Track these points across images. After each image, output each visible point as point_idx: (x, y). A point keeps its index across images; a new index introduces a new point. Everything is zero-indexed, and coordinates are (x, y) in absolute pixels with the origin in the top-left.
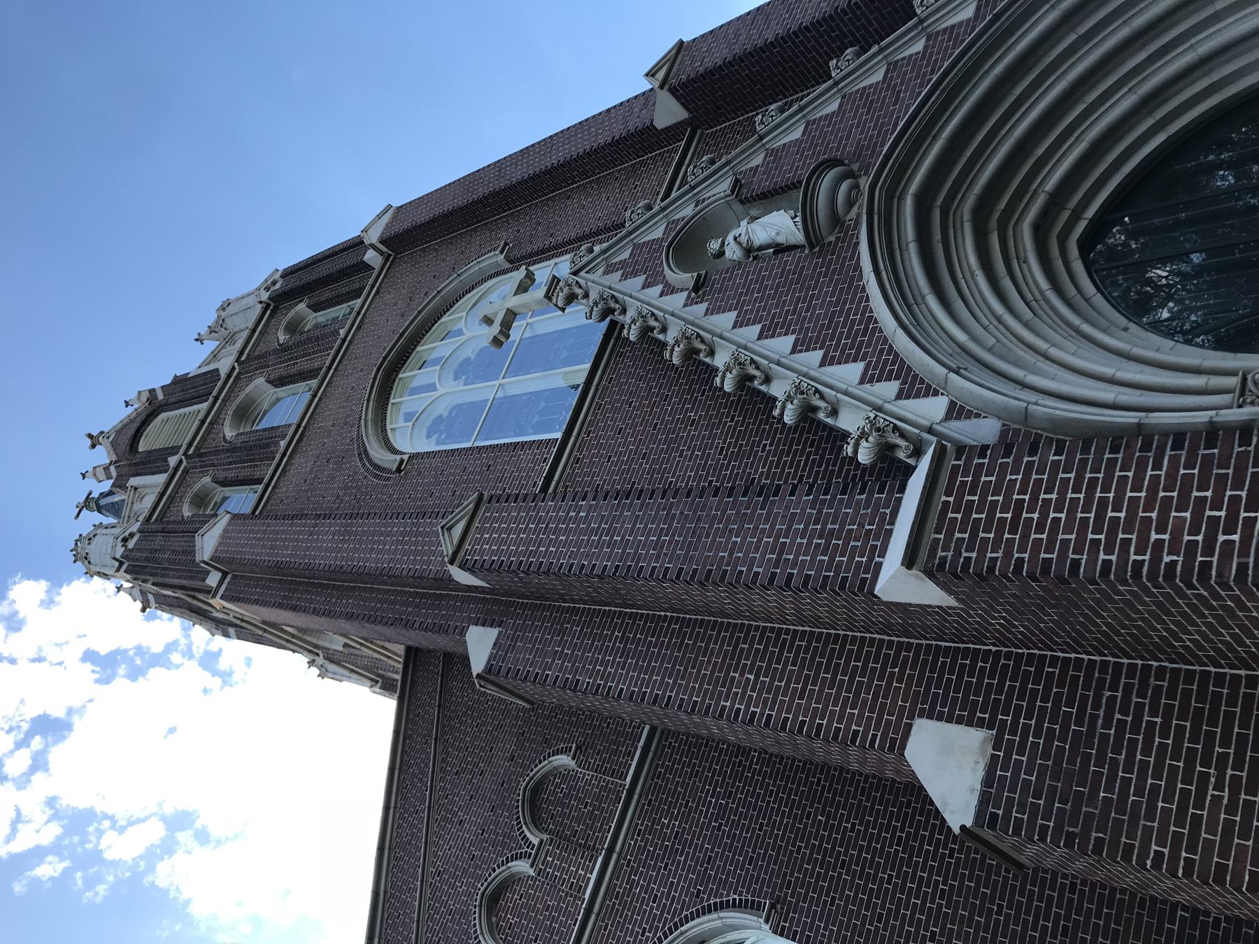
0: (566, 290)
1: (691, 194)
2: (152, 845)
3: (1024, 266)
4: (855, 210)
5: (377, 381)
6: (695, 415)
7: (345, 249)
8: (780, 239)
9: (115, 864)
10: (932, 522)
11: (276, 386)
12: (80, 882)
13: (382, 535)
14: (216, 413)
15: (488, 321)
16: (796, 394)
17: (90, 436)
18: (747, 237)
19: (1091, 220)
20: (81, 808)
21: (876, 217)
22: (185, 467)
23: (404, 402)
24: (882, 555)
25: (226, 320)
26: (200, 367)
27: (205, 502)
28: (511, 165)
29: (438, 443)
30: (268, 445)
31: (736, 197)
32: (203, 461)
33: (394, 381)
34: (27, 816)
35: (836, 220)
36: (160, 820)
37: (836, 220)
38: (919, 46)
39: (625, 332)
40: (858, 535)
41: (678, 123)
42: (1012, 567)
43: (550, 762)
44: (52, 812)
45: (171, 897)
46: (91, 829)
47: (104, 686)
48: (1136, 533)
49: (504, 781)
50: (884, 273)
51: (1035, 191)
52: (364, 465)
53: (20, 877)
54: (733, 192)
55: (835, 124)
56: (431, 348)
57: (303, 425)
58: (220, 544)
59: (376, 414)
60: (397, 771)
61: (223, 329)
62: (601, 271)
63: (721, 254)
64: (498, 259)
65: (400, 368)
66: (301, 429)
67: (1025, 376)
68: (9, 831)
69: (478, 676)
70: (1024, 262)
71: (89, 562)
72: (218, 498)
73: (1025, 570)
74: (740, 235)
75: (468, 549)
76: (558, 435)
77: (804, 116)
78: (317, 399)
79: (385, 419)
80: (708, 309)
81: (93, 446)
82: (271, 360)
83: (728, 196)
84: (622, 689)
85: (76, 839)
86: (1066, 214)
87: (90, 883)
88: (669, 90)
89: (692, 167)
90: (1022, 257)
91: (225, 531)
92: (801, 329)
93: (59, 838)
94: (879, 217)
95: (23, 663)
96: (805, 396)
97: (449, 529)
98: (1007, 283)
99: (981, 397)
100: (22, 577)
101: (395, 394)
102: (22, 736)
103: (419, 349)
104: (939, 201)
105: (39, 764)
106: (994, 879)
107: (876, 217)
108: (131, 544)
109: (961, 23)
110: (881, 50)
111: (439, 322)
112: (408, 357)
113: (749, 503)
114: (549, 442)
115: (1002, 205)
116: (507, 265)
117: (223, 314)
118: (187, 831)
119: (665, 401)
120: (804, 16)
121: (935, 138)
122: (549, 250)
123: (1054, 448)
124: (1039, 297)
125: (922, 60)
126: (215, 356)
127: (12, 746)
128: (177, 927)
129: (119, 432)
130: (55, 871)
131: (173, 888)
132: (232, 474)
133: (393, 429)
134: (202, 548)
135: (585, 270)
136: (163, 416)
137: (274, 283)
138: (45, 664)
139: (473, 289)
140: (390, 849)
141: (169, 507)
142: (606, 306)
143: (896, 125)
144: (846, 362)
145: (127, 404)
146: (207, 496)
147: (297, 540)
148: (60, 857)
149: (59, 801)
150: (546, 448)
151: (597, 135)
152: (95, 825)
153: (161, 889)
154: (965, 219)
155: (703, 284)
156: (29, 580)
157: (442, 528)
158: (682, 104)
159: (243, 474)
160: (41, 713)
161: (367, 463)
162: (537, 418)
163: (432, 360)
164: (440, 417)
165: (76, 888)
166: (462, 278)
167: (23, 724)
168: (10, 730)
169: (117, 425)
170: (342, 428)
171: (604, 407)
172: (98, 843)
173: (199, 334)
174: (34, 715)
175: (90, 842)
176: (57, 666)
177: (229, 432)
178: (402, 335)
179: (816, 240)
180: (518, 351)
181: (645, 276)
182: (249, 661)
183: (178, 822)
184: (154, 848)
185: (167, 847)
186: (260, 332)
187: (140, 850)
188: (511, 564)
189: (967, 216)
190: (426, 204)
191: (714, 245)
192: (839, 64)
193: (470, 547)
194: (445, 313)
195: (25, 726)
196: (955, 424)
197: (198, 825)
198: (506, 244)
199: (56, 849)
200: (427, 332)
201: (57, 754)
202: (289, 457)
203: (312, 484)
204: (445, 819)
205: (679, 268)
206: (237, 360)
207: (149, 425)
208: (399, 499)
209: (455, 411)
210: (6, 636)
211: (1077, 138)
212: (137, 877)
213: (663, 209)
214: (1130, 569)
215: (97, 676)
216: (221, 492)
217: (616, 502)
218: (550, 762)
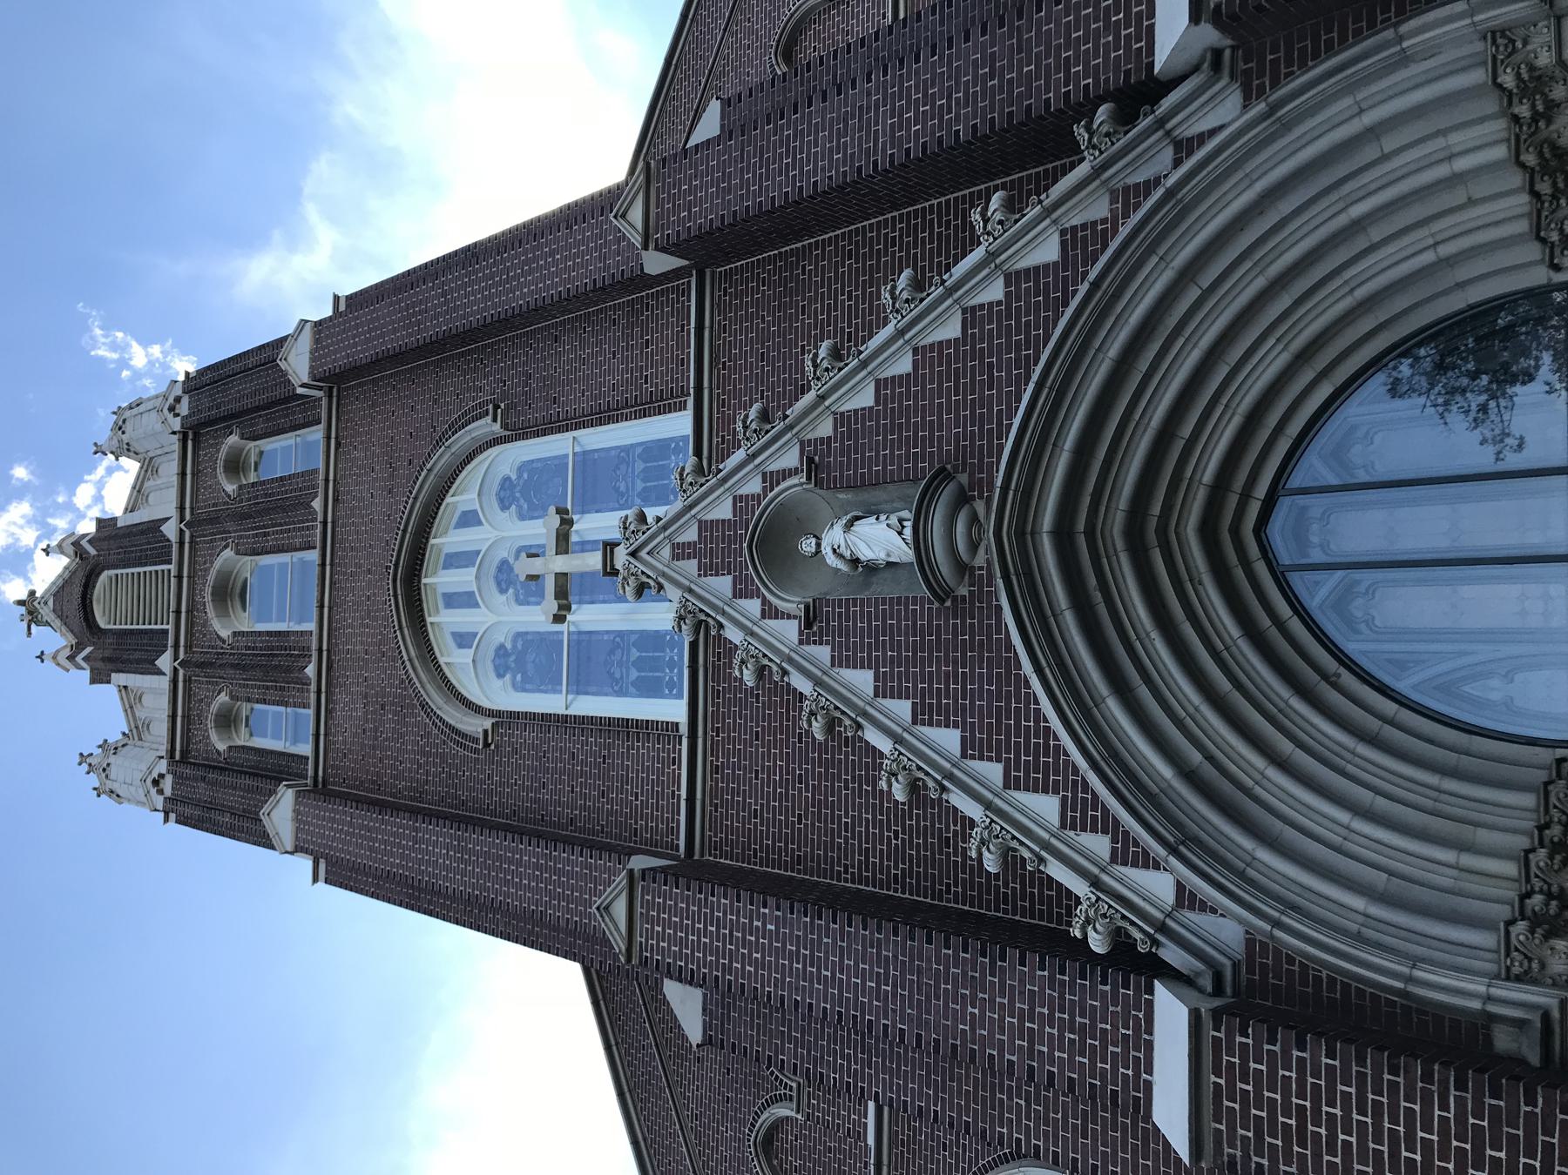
3: (1200, 588)
4: (981, 551)
5: (400, 597)
17: (81, 754)
22: (185, 675)
27: (232, 718)
33: (419, 589)
35: (962, 568)
37: (962, 568)
50: (1047, 671)
57: (325, 647)
59: (418, 646)
65: (420, 570)
66: (325, 653)
71: (107, 776)
74: (839, 547)
88: (657, 249)
94: (1017, 575)
104: (1081, 526)
112: (424, 555)
123: (1324, 1047)
133: (431, 623)
140: (630, 1091)
155: (815, 618)
157: (598, 908)
158: (678, 256)
162: (634, 674)
166: (453, 450)
178: (405, 531)
179: (945, 594)
186: (193, 474)
189: (1120, 544)
194: (447, 492)
200: (434, 518)
202: (326, 692)
204: (679, 1056)
207: (94, 587)
216: (245, 708)
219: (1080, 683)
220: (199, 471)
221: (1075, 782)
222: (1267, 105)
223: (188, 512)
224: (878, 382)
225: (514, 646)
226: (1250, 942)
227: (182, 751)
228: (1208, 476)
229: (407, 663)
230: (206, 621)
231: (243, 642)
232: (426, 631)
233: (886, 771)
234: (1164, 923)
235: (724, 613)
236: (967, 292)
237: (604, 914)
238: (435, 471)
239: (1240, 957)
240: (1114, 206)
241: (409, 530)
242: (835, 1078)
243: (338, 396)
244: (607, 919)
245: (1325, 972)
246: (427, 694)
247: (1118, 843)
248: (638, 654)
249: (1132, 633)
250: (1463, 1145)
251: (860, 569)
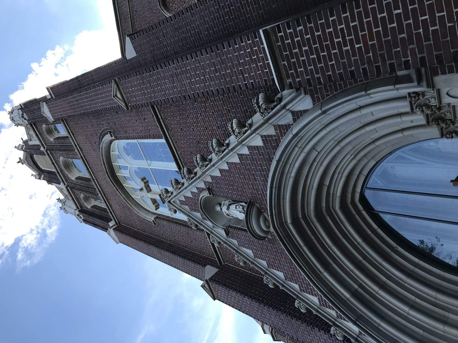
7: (103, 228)
37: (267, 233)
48: (339, 29)
59: (124, 194)
67: (379, 290)
71: (64, 205)
78: (95, 180)
104: (300, 216)
112: (113, 167)
141: (79, 201)
146: (66, 161)
155: (229, 232)
180: (144, 153)
182: (56, 75)
186: (40, 134)
189: (315, 220)
200: (110, 158)
202: (107, 201)
227: (80, 206)
228: (339, 193)
238: (103, 148)
241: (105, 163)
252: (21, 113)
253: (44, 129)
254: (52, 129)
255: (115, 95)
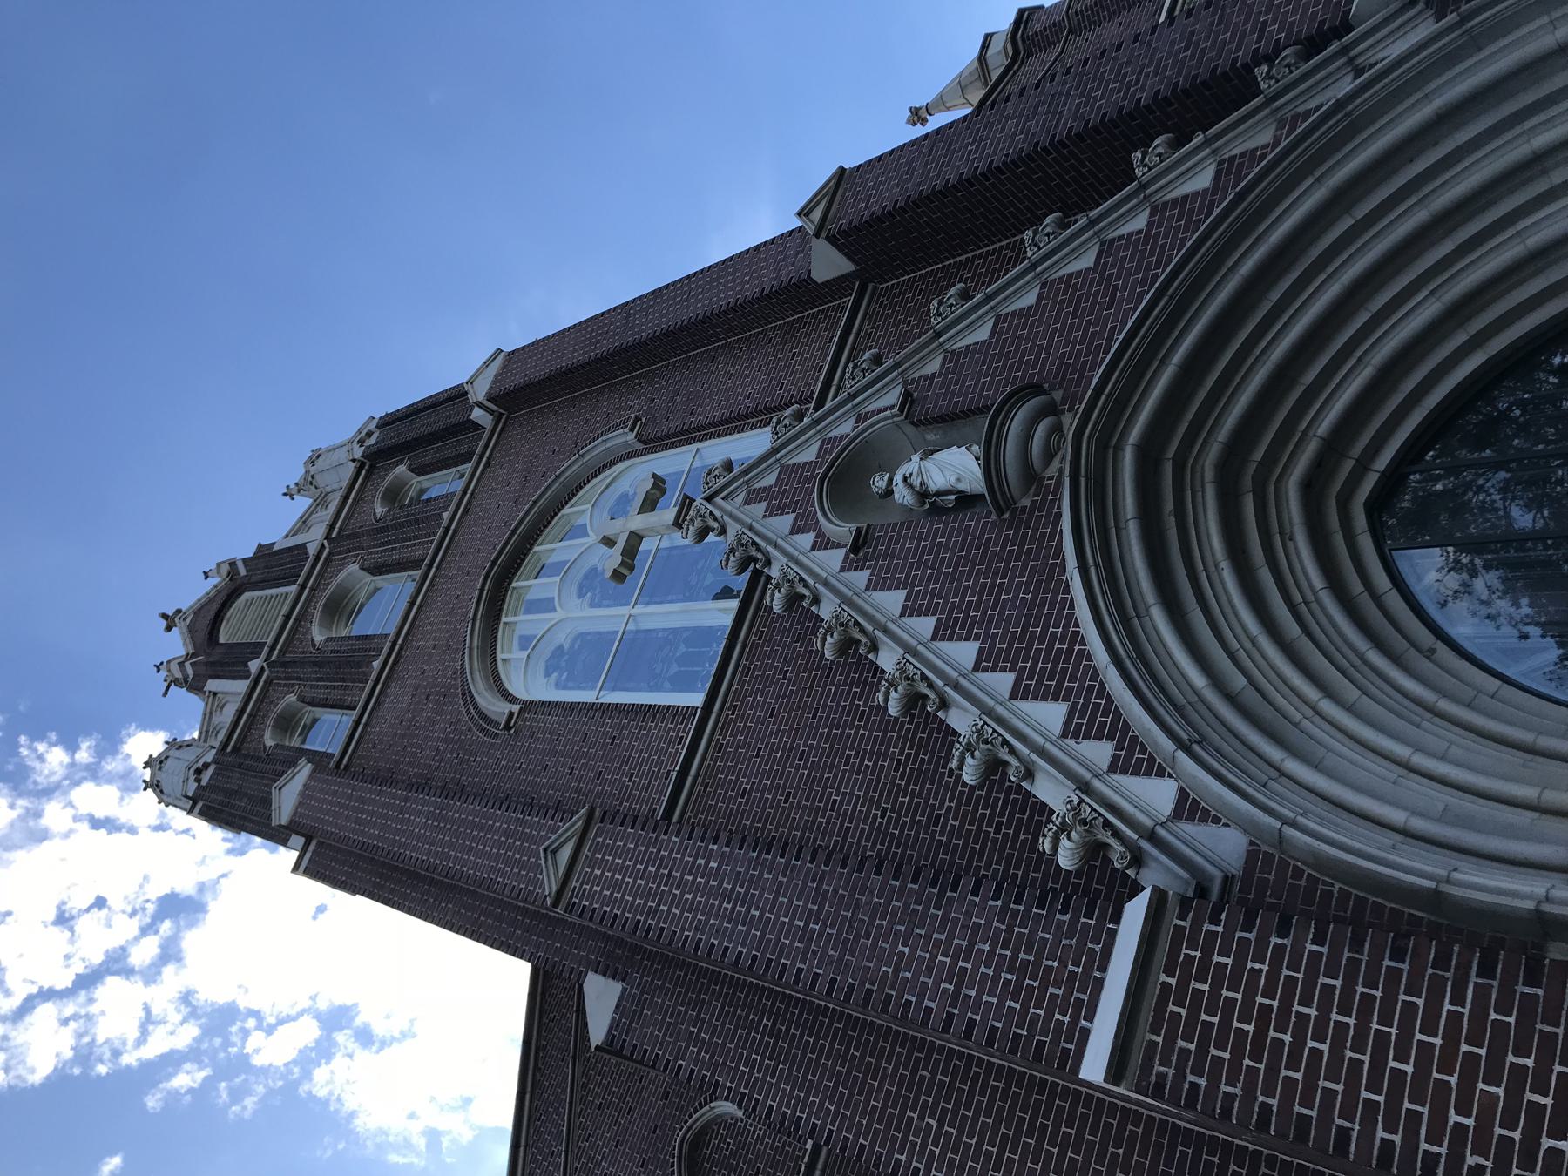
0: (698, 522)
1: (849, 406)
2: (306, 1047)
3: (1290, 544)
4: (1056, 463)
6: (865, 706)
7: (450, 399)
8: (962, 487)
9: (265, 1071)
10: (1147, 1014)
11: (372, 574)
12: (224, 1095)
13: (481, 830)
14: (302, 608)
15: (609, 542)
16: (978, 742)
17: (165, 616)
18: (920, 479)
19: (1383, 474)
20: (221, 1003)
21: (1083, 481)
22: (268, 677)
23: (518, 622)
24: (1090, 1017)
25: (316, 477)
26: (287, 536)
28: (641, 311)
29: (558, 686)
30: (358, 665)
31: (906, 418)
32: (288, 672)
33: (507, 591)
34: (158, 1015)
35: (1031, 477)
36: (314, 1018)
37: (1031, 477)
38: (1140, 222)
39: (768, 599)
40: (1059, 979)
41: (843, 276)
42: (1255, 1116)
43: (712, 1108)
44: (188, 1010)
45: (332, 1109)
46: (234, 1029)
47: (239, 858)
49: (656, 1126)
50: (1093, 570)
51: (1305, 433)
52: (468, 711)
53: (153, 1091)
54: (901, 410)
55: (1032, 326)
56: (549, 549)
57: (400, 642)
58: (300, 804)
59: (483, 638)
60: (528, 1096)
61: (313, 488)
62: (740, 499)
63: (889, 492)
64: (628, 438)
65: (514, 574)
66: (397, 647)
67: (1282, 760)
68: (138, 1034)
69: (597, 1048)
70: (1291, 540)
72: (306, 720)
73: (1273, 1127)
74: (911, 475)
75: (575, 887)
76: (696, 699)
77: (992, 308)
78: (415, 607)
79: (495, 645)
80: (870, 580)
81: (169, 628)
82: (366, 541)
83: (895, 415)
84: (771, 1107)
85: (217, 1041)
86: (1348, 465)
87: (237, 1095)
88: (827, 239)
89: (851, 365)
90: (1288, 531)
91: (306, 786)
92: (987, 634)
93: (197, 1040)
95: (144, 833)
96: (989, 746)
97: (554, 852)
98: (1265, 576)
99: (1220, 798)
100: (137, 728)
101: (507, 610)
102: (148, 920)
103: (536, 549)
104: (1171, 452)
105: (170, 954)
106: (1312, 1049)
107: (1083, 481)
108: (206, 777)
109: (1195, 194)
110: (1092, 223)
111: (560, 515)
112: (523, 560)
113: (920, 894)
114: (688, 711)
115: (1258, 455)
116: (640, 446)
117: (313, 470)
118: (346, 1031)
119: (828, 677)
120: (995, 152)
121: (1163, 362)
122: (689, 431)
123: (1312, 930)
124: (1310, 597)
125: (1146, 242)
126: (304, 522)
127: (136, 932)
128: (340, 1147)
129: (199, 611)
130: (194, 1082)
131: (333, 1098)
132: (321, 694)
133: (503, 660)
134: (279, 807)
135: (721, 496)
136: (247, 595)
137: (369, 434)
138: (170, 832)
139: (600, 473)
142: (746, 554)
143: (1110, 340)
144: (1044, 699)
145: (206, 575)
147: (386, 817)
148: (198, 1063)
149: (196, 996)
150: (682, 723)
151: (743, 283)
152: (239, 1023)
153: (320, 1099)
154: (1207, 480)
155: (865, 542)
156: (145, 730)
158: (845, 254)
159: (335, 695)
160: (169, 891)
161: (471, 708)
162: (674, 668)
163: (553, 564)
164: (561, 647)
165: (220, 1101)
167: (149, 906)
168: (133, 913)
169: (203, 597)
170: (444, 653)
171: (753, 674)
172: (243, 1047)
173: (288, 487)
174: (161, 893)
175: (234, 1045)
176: (184, 835)
177: (318, 635)
179: (1005, 502)
181: (794, 515)
183: (336, 1019)
184: (308, 1052)
185: (323, 1051)
186: (354, 500)
187: (291, 1054)
188: (626, 922)
189: (1209, 475)
190: (542, 353)
191: (879, 482)
192: (1037, 239)
193: (578, 885)
194: (566, 503)
195: (151, 908)
196: (1187, 828)
197: (358, 1022)
198: (637, 419)
199: (192, 1055)
200: (546, 527)
201: (192, 941)
202: (384, 684)
203: (409, 728)
205: (834, 510)
206: (327, 537)
207: (231, 606)
208: (506, 769)
209: (579, 642)
210: (122, 799)
211: (1360, 359)
212: (291, 1087)
213: (817, 422)
214: (1419, 1164)
215: (229, 845)
216: (310, 712)
217: (755, 854)
218: (712, 1108)
219: (1126, 593)
220: (361, 499)
221: (1091, 688)
222: (1459, 15)
223: (336, 531)
224: (998, 317)
225: (572, 647)
226: (1252, 856)
228: (1324, 427)
229: (467, 650)
230: (309, 629)
231: (332, 644)
232: (497, 629)
233: (886, 681)
234: (1153, 832)
235: (776, 546)
236: (1111, 223)
237: (549, 857)
239: (1234, 872)
240: (1279, 133)
242: (730, 1088)
243: (505, 423)
244: (550, 861)
245: (1338, 885)
246: (473, 679)
247: (1122, 750)
248: (685, 650)
249: (1199, 561)
250: (1476, 1050)
251: (927, 506)
252: (209, 757)
253: (281, 706)
254: (301, 719)
255: (551, 849)
